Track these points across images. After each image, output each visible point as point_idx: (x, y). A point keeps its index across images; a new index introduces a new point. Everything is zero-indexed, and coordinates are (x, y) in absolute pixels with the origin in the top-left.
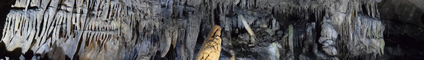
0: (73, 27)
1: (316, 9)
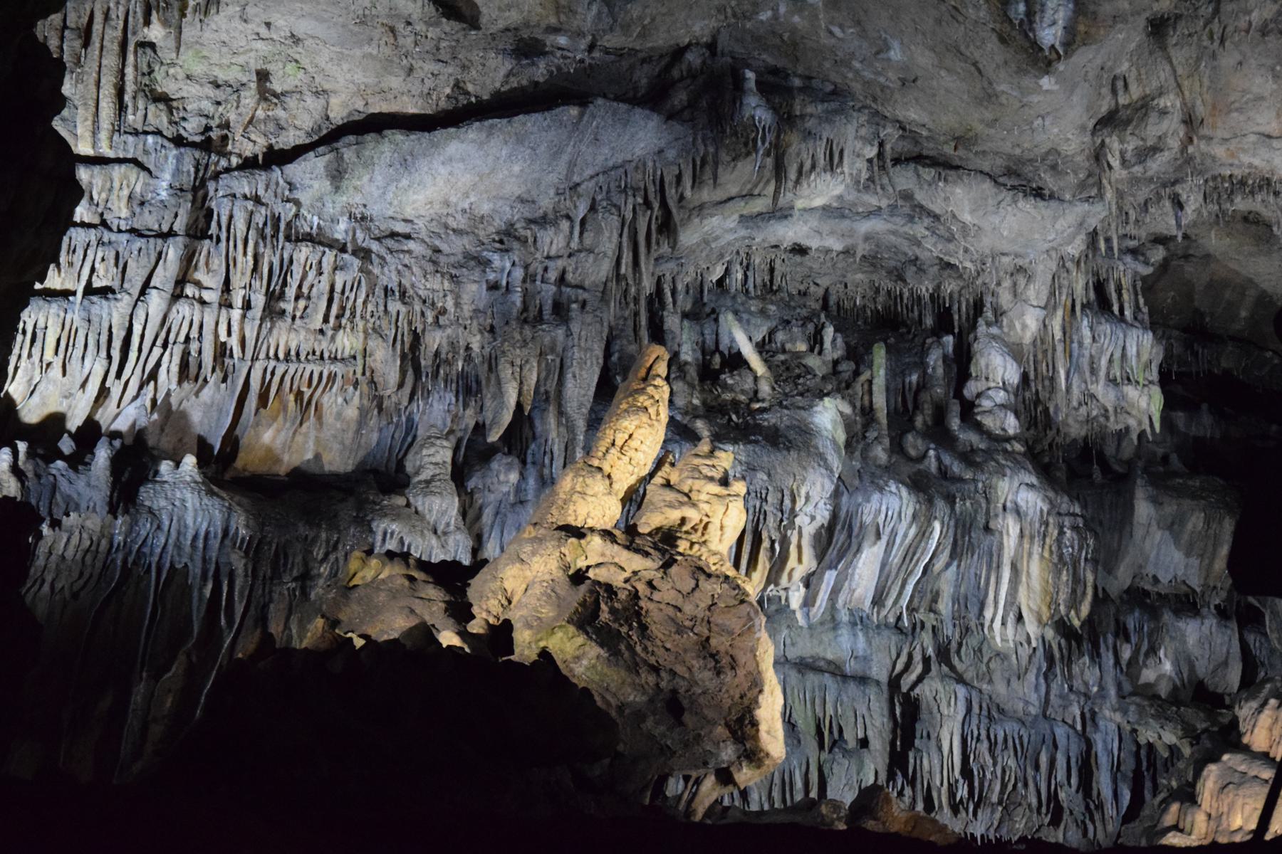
0: (222, 351)
1: (956, 296)
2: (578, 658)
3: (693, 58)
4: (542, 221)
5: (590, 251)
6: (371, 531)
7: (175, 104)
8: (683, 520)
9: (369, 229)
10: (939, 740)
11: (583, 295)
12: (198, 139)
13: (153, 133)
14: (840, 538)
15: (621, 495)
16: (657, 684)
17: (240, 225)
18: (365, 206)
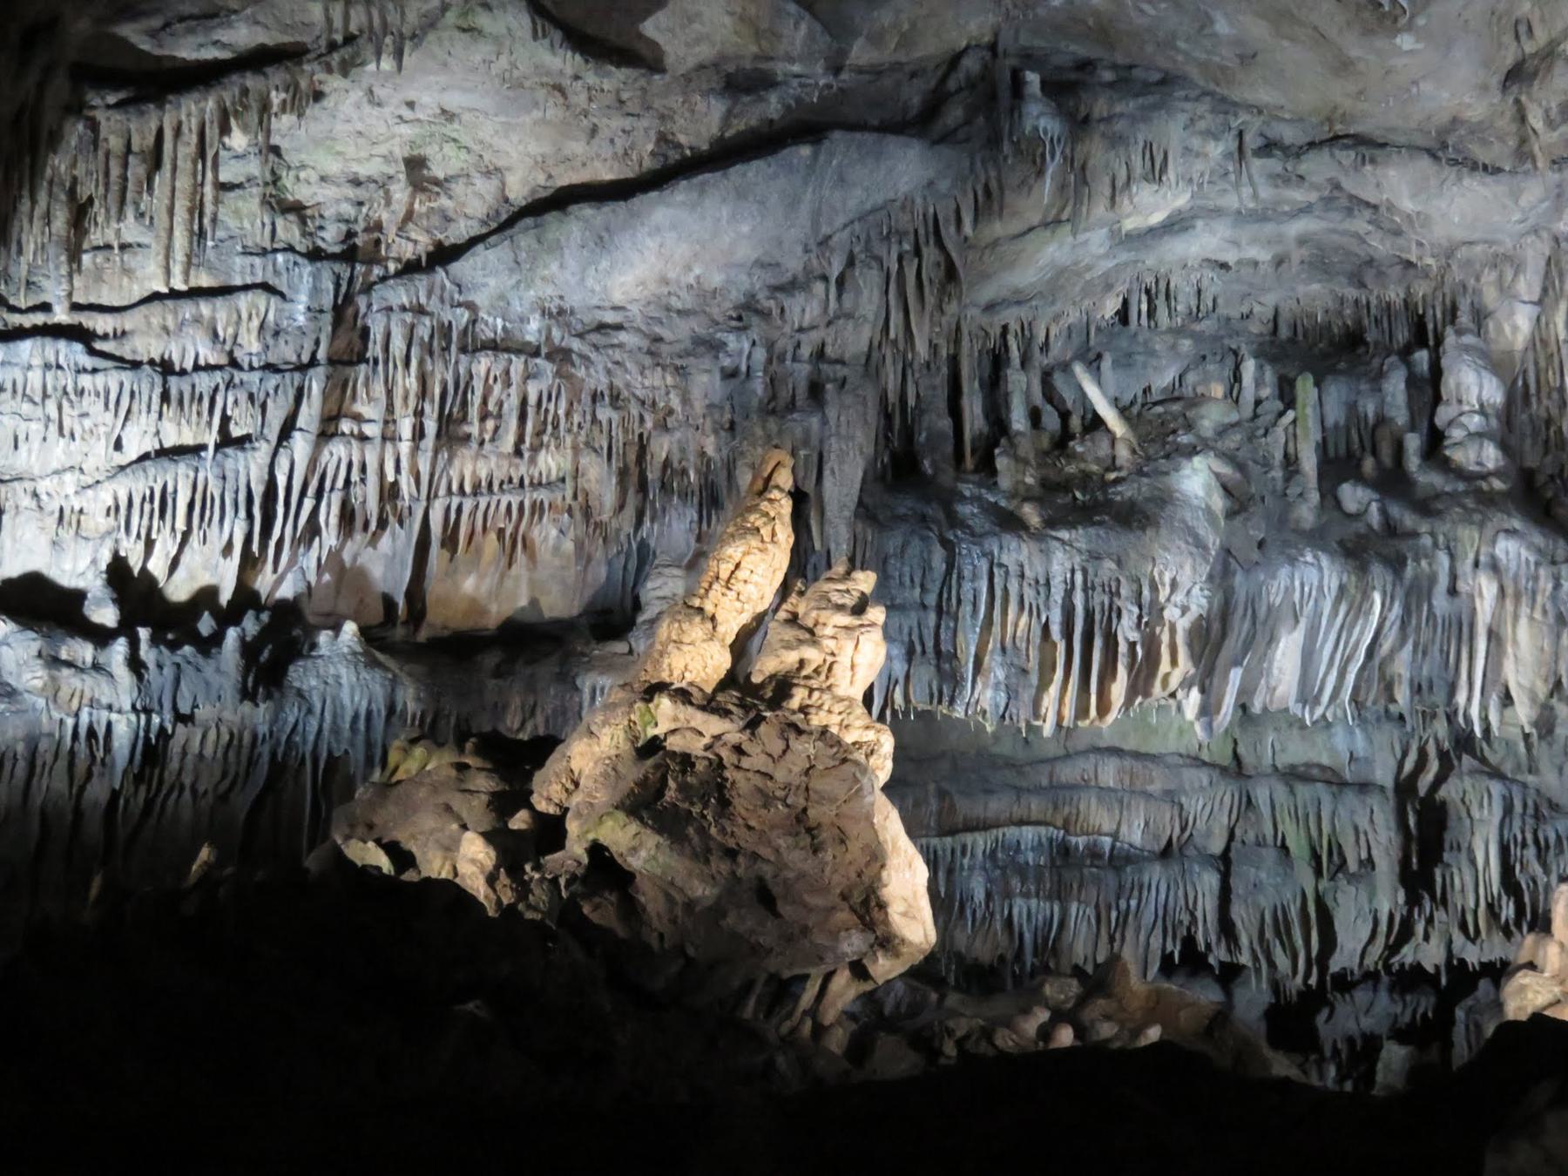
0: (390, 493)
1: (1429, 299)
2: (634, 850)
3: (971, 64)
4: (791, 287)
5: (849, 316)
6: (577, 689)
7: (309, 212)
8: (802, 663)
9: (568, 325)
10: (1471, 851)
11: (841, 371)
12: (337, 249)
13: (284, 250)
14: (1240, 628)
15: (730, 639)
16: (733, 873)
17: (398, 345)
18: (561, 298)
